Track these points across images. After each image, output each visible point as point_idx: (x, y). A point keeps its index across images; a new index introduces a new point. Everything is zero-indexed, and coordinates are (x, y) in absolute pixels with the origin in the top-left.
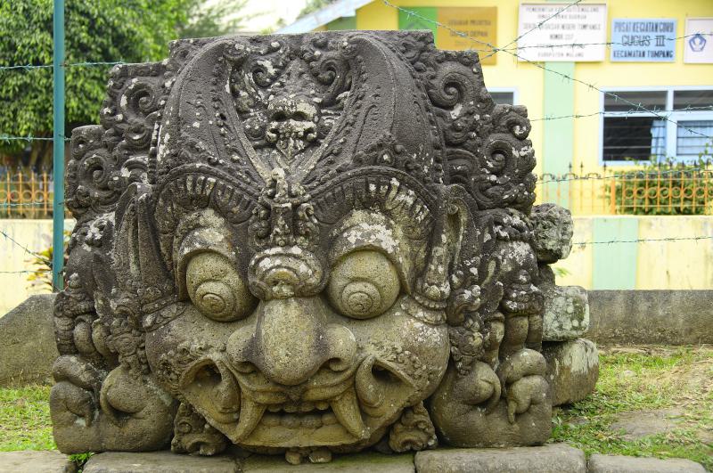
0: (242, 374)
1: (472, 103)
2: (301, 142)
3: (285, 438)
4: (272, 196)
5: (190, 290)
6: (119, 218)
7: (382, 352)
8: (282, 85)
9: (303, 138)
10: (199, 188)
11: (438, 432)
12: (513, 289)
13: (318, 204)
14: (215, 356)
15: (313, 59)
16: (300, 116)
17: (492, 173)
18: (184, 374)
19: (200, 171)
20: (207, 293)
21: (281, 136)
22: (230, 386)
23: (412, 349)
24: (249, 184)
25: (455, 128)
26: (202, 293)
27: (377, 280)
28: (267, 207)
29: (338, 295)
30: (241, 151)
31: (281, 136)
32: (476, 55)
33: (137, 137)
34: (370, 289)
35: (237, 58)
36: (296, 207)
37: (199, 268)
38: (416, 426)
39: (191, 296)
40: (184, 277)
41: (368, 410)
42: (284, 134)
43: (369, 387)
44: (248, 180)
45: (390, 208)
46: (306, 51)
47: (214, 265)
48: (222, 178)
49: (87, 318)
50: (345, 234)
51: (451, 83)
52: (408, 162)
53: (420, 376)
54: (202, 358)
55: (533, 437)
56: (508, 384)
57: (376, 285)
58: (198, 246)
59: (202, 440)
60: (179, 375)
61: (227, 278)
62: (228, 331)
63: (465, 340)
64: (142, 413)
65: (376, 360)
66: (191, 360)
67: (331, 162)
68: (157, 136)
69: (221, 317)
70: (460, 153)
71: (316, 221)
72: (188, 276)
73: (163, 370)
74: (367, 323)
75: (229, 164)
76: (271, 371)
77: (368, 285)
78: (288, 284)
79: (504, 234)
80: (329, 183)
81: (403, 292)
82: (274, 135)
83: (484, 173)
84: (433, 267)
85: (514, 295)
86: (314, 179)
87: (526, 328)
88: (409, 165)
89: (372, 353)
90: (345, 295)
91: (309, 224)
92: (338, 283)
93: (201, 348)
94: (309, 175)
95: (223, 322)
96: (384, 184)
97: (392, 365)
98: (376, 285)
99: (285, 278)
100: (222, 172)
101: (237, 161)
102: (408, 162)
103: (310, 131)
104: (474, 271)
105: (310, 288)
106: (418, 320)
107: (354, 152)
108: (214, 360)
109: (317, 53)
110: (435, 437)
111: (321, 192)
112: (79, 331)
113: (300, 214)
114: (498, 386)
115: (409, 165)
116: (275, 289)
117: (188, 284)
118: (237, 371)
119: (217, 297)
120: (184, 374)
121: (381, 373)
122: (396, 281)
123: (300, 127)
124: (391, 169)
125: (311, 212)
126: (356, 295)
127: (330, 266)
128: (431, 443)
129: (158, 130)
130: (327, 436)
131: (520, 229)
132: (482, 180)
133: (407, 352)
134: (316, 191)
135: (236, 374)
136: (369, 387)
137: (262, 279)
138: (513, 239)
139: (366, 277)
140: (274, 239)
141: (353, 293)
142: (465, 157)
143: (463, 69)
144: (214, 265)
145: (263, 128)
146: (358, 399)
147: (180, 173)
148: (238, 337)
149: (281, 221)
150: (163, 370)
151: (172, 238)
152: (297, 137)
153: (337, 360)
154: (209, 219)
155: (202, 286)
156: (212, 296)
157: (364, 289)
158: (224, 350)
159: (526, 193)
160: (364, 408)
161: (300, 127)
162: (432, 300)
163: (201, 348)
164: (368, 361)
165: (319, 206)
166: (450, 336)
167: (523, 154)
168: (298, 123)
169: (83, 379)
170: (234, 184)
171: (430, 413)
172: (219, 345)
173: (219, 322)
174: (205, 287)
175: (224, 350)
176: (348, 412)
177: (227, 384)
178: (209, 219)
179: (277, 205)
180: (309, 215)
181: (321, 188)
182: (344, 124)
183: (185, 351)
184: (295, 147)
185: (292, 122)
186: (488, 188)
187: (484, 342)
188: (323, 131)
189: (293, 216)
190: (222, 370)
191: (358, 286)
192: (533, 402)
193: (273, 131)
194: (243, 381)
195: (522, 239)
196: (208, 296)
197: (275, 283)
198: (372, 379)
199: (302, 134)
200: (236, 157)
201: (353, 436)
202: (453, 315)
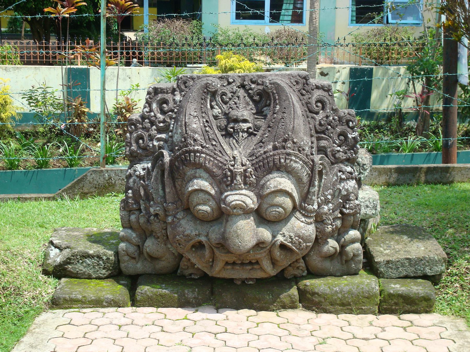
0: (216, 247)
1: (329, 111)
2: (246, 134)
6: (153, 167)
7: (285, 238)
9: (247, 132)
10: (197, 159)
11: (308, 269)
12: (347, 203)
13: (255, 168)
14: (203, 239)
15: (251, 89)
16: (245, 121)
17: (338, 146)
19: (198, 151)
22: (210, 252)
23: (299, 237)
25: (320, 124)
28: (230, 171)
30: (216, 140)
31: (236, 132)
32: (330, 86)
33: (161, 125)
34: (280, 210)
35: (213, 90)
36: (245, 171)
38: (298, 268)
42: (237, 130)
43: (277, 253)
44: (221, 155)
46: (247, 85)
48: (211, 156)
49: (137, 213)
50: (268, 183)
51: (319, 101)
54: (196, 239)
55: (353, 271)
56: (343, 247)
58: (196, 188)
62: (209, 226)
63: (324, 230)
64: (164, 259)
65: (282, 242)
66: (191, 240)
67: (261, 147)
68: (173, 127)
70: (322, 137)
71: (254, 177)
75: (211, 147)
76: (232, 249)
78: (241, 208)
79: (343, 177)
80: (261, 158)
82: (232, 130)
83: (334, 146)
84: (310, 197)
85: (348, 206)
86: (253, 155)
87: (352, 221)
90: (268, 213)
91: (251, 179)
92: (265, 206)
96: (288, 159)
100: (208, 152)
101: (215, 145)
103: (250, 128)
104: (329, 197)
106: (302, 222)
109: (253, 86)
110: (306, 272)
111: (257, 162)
112: (133, 217)
113: (247, 174)
114: (338, 249)
116: (235, 211)
123: (245, 126)
124: (292, 151)
125: (252, 173)
128: (305, 274)
131: (351, 173)
132: (333, 150)
133: (296, 238)
134: (254, 162)
135: (213, 248)
136: (277, 253)
138: (348, 179)
142: (326, 139)
143: (326, 94)
144: (204, 196)
146: (271, 257)
147: (187, 152)
148: (214, 233)
149: (238, 178)
152: (243, 131)
153: (263, 243)
154: (201, 174)
159: (354, 155)
160: (274, 262)
161: (245, 126)
164: (279, 243)
165: (256, 170)
166: (316, 227)
167: (353, 136)
168: (244, 124)
169: (135, 241)
170: (214, 158)
171: (305, 262)
174: (200, 207)
178: (201, 174)
179: (236, 170)
180: (251, 175)
181: (257, 160)
183: (188, 236)
184: (243, 137)
185: (241, 124)
186: (336, 153)
187: (333, 229)
188: (257, 128)
189: (245, 175)
192: (354, 255)
193: (231, 128)
194: (217, 252)
195: (352, 178)
196: (200, 211)
197: (235, 208)
198: (279, 250)
199: (246, 130)
200: (214, 143)
202: (319, 220)
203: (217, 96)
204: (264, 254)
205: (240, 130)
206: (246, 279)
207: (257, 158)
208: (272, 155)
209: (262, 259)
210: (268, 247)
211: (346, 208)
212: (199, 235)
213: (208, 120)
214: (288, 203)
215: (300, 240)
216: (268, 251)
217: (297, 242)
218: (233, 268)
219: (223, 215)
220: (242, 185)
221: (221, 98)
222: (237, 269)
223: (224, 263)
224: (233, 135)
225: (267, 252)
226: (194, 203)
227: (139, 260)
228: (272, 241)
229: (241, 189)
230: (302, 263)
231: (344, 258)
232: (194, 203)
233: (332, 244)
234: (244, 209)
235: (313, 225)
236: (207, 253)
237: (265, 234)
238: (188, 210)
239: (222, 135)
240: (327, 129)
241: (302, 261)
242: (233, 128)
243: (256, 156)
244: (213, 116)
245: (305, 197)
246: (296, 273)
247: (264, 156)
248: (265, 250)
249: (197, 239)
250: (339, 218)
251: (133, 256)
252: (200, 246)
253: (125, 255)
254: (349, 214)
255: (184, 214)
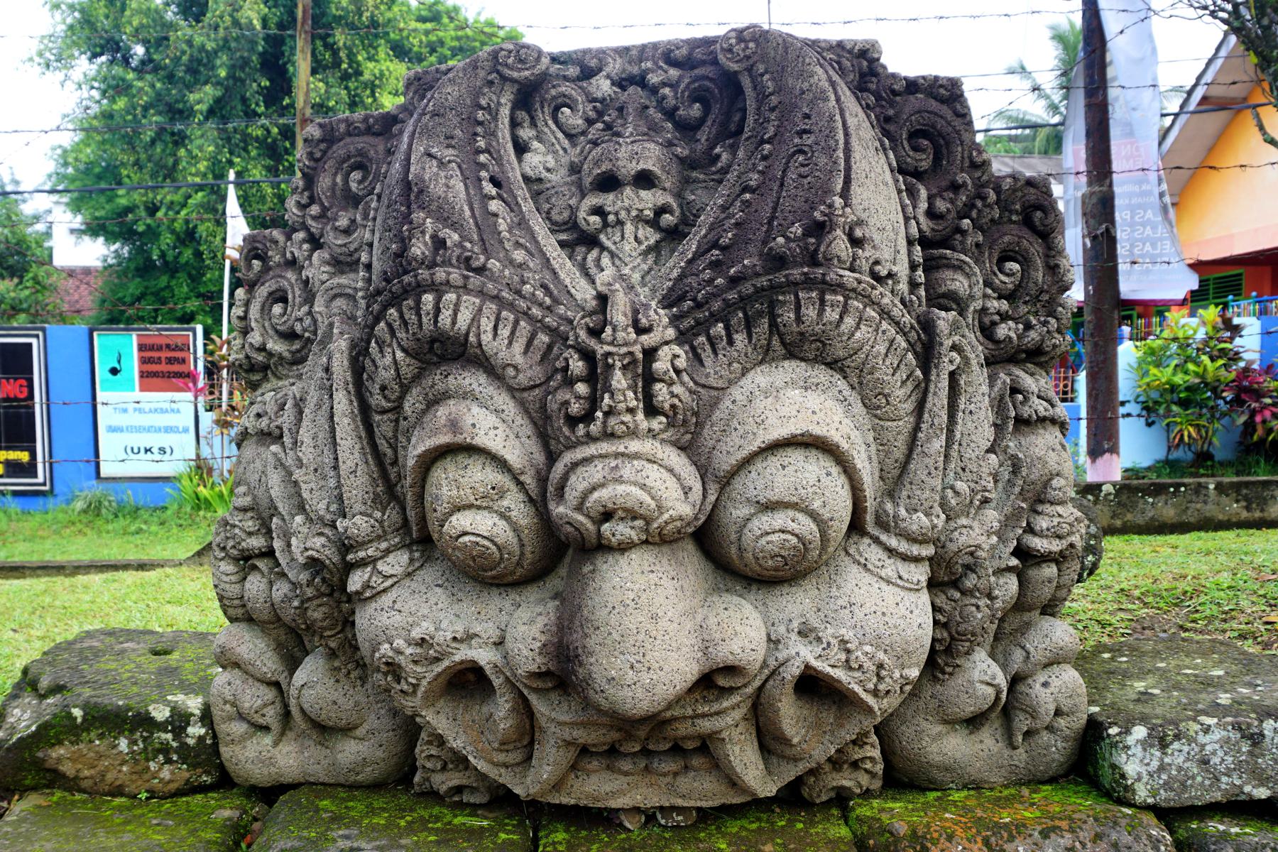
0: (536, 690)
3: (622, 793)
4: (596, 333)
5: (433, 527)
7: (819, 650)
8: (608, 127)
9: (654, 223)
14: (484, 656)
18: (424, 683)
20: (465, 534)
21: (611, 218)
22: (513, 709)
24: (548, 308)
26: (453, 532)
27: (816, 505)
28: (588, 356)
29: (733, 537)
37: (450, 482)
39: (435, 536)
40: (420, 497)
41: (773, 745)
43: (790, 715)
44: (548, 301)
45: (841, 353)
47: (479, 476)
52: (877, 262)
53: (888, 692)
54: (457, 658)
56: (128, 193)
57: (814, 516)
59: (465, 782)
60: (416, 687)
61: (505, 503)
62: (507, 604)
65: (807, 666)
66: (437, 660)
69: (494, 577)
72: (428, 498)
73: (386, 674)
74: (786, 589)
77: (801, 517)
80: (716, 305)
81: (856, 527)
88: (878, 268)
89: (803, 654)
90: (748, 536)
91: (677, 389)
93: (455, 639)
94: (671, 289)
95: (498, 586)
97: (839, 674)
98: (814, 516)
99: (629, 505)
102: (877, 262)
105: (678, 524)
107: (765, 243)
108: (482, 663)
114: (1004, 686)
115: (878, 268)
116: (606, 527)
117: (431, 516)
118: (526, 686)
119: (486, 543)
120: (424, 683)
121: (812, 686)
122: (849, 503)
126: (774, 538)
127: (722, 481)
129: (376, 210)
130: (701, 789)
135: (525, 692)
136: (790, 715)
137: (579, 508)
139: (795, 499)
140: (604, 423)
141: (769, 534)
144: (479, 476)
145: (573, 210)
149: (619, 380)
150: (386, 674)
151: (397, 421)
153: (731, 670)
155: (454, 519)
156: (473, 538)
157: (792, 526)
158: (500, 643)
160: (770, 743)
162: (912, 539)
163: (455, 639)
164: (794, 670)
172: (488, 630)
173: (492, 585)
174: (462, 521)
175: (500, 643)
176: (745, 759)
177: (507, 706)
182: (737, 189)
190: (497, 681)
191: (780, 519)
194: (540, 706)
196: (466, 539)
199: (649, 213)
201: (744, 790)
203: (537, 105)
204: (737, 714)
205: (628, 211)
206: (662, 808)
207: (699, 305)
208: (763, 289)
209: (724, 735)
210: (749, 690)
211: (1039, 534)
212: (469, 637)
213: (500, 176)
214: (835, 500)
215: (881, 656)
216: (749, 703)
217: (869, 665)
218: (608, 768)
219: (560, 554)
220: (640, 416)
221: (556, 122)
222: (626, 774)
223: (571, 754)
224: (603, 237)
225: (744, 710)
226: (442, 508)
227: (282, 734)
228: (765, 664)
229: (633, 433)
230: (873, 746)
231: (1022, 723)
232: (442, 508)
233: (982, 673)
234: (648, 522)
235: (925, 598)
236: (502, 708)
237: (743, 628)
238: (422, 540)
239: (562, 244)
240: (959, 230)
241: (874, 738)
242: (599, 211)
243: (694, 300)
244: (527, 179)
245: (897, 478)
246: (847, 783)
247: (732, 296)
248: (735, 699)
249: (464, 653)
250: (1009, 569)
251: (261, 721)
252: (467, 682)
253: (230, 719)
254: (1046, 558)
255: (412, 560)
